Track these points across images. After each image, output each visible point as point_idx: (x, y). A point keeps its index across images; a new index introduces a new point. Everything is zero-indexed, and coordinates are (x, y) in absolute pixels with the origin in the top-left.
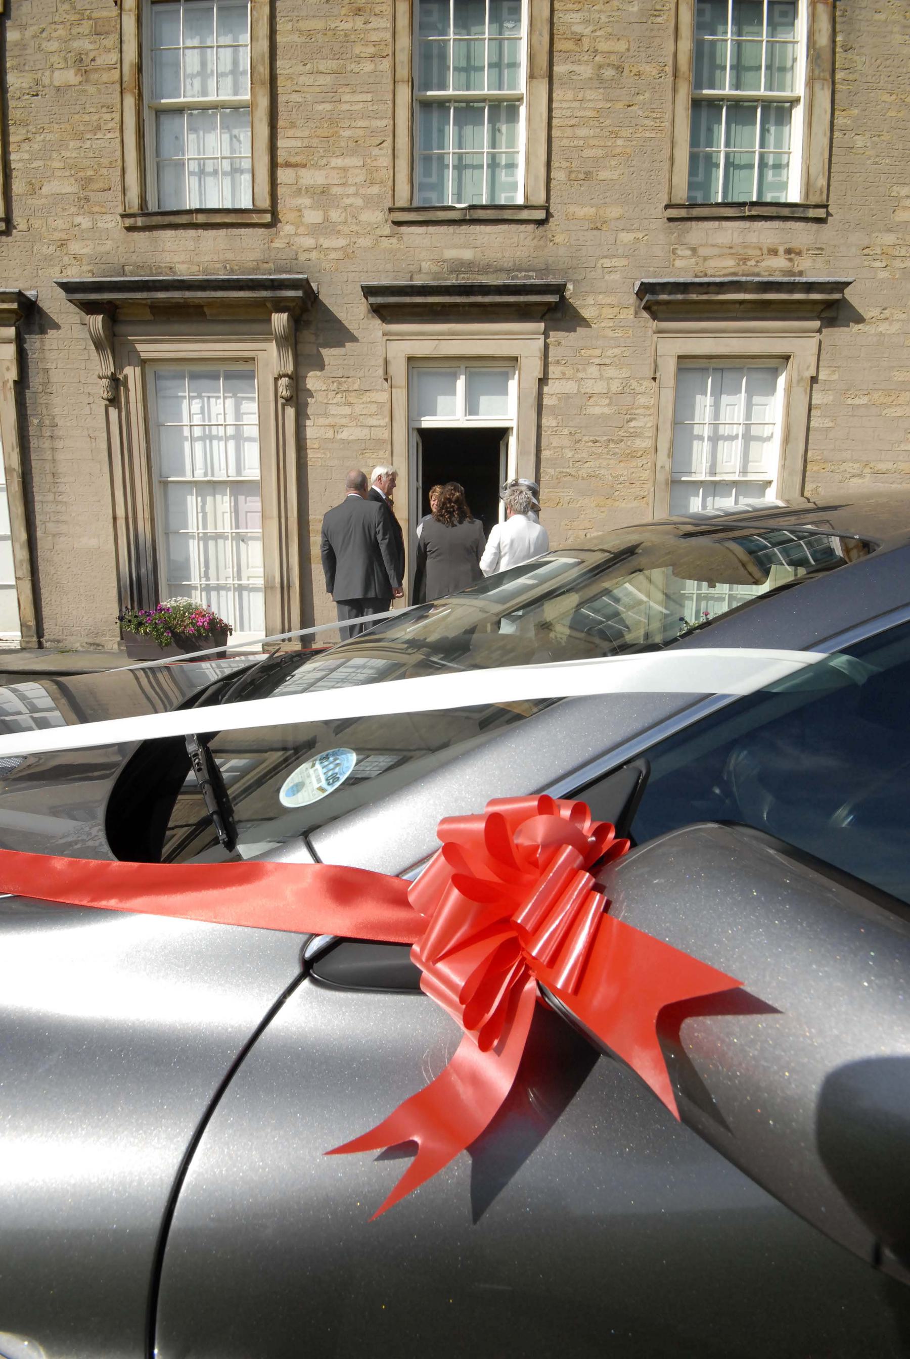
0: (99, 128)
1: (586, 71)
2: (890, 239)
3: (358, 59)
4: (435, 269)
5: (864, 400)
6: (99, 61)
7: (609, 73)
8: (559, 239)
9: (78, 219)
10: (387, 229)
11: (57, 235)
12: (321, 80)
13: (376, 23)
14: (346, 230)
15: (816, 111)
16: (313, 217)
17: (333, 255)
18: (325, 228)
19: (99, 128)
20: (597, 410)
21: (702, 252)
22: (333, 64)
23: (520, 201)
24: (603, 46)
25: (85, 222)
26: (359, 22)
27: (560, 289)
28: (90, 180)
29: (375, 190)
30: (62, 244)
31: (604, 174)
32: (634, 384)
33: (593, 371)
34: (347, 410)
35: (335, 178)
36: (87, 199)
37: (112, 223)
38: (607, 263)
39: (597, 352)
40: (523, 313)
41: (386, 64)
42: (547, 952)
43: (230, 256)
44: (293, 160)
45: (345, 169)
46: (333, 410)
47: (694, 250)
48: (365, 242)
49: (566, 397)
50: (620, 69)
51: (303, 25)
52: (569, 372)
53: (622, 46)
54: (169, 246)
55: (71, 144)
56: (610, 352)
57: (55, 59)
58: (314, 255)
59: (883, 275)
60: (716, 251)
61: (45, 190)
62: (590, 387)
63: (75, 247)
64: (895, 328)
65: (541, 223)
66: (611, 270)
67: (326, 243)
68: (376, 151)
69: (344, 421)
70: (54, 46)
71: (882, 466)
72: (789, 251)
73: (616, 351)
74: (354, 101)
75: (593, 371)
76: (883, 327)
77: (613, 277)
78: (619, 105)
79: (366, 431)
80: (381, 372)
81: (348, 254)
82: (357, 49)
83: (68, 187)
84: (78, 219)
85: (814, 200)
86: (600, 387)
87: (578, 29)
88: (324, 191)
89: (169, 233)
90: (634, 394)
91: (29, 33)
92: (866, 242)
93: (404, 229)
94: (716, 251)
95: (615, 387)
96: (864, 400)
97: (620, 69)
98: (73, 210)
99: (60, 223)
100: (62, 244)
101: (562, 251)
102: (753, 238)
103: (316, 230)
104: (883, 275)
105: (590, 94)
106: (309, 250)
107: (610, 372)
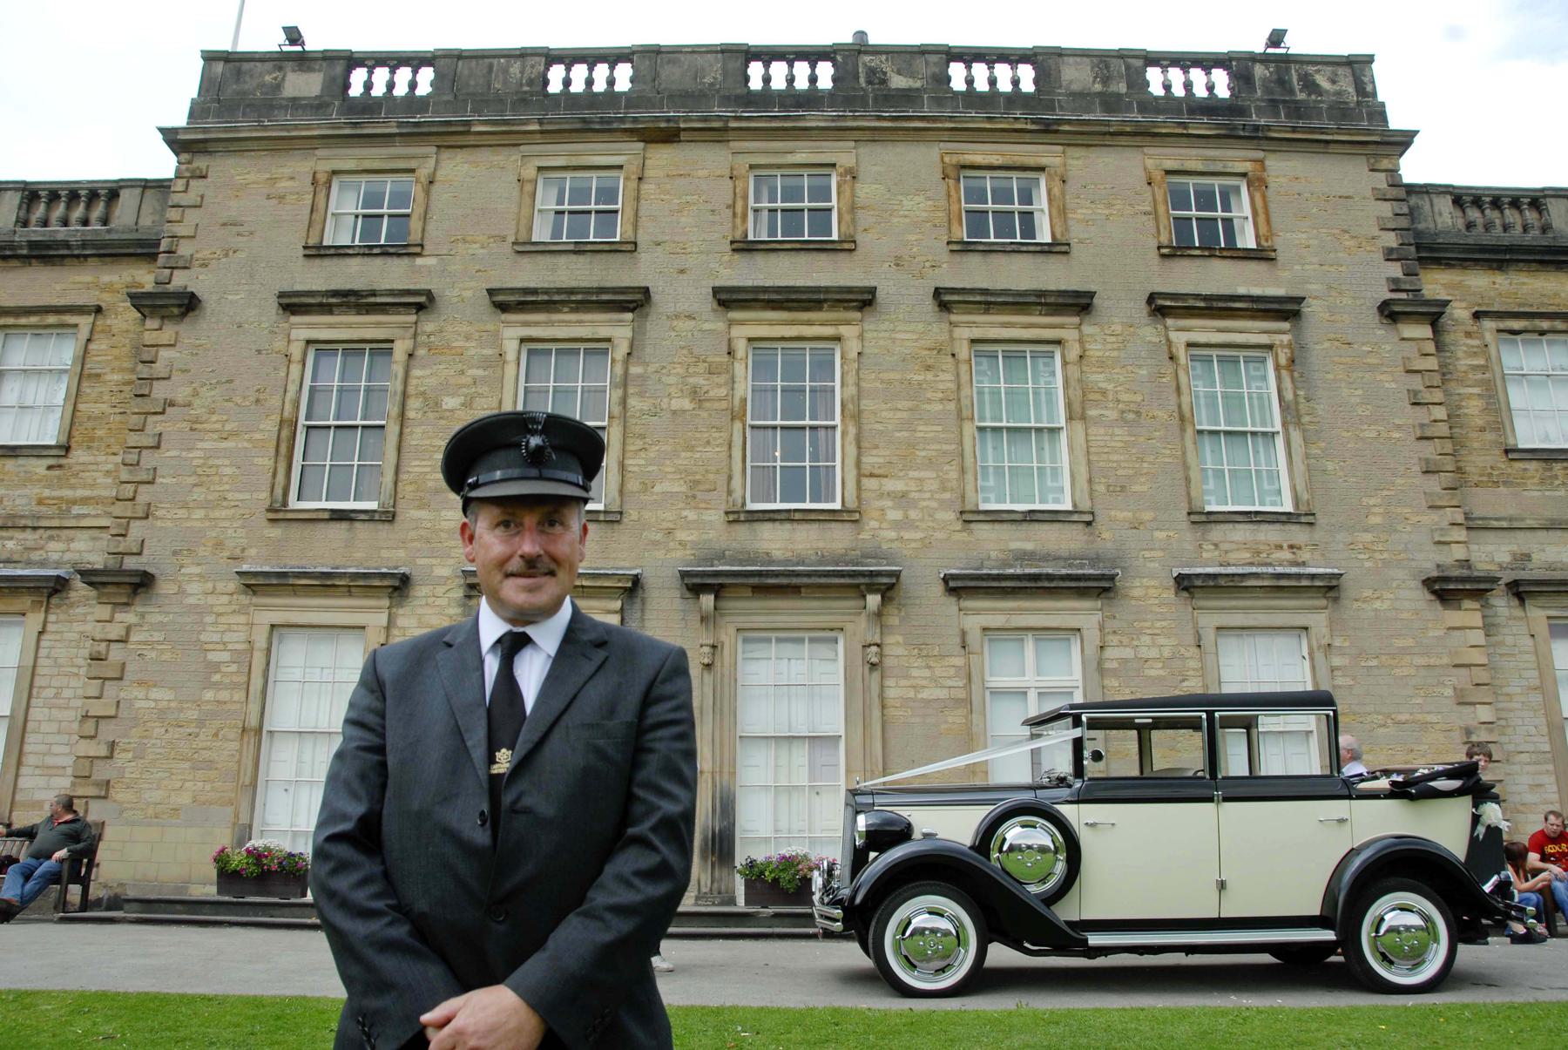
0: (708, 443)
1: (1112, 415)
2: (1368, 537)
3: (929, 401)
4: (1001, 556)
5: (1374, 663)
6: (711, 394)
7: (1131, 416)
8: (1106, 535)
9: (685, 513)
10: (959, 526)
11: (665, 525)
12: (899, 415)
13: (943, 376)
14: (924, 525)
15: (1293, 445)
16: (895, 515)
17: (913, 545)
18: (906, 524)
19: (708, 443)
20: (1153, 673)
21: (1224, 546)
22: (910, 404)
23: (1069, 507)
24: (1124, 397)
25: (691, 515)
26: (929, 376)
27: (1112, 578)
28: (697, 482)
29: (947, 496)
30: (669, 532)
31: (1136, 488)
32: (1183, 650)
33: (1146, 639)
34: (927, 673)
35: (913, 486)
36: (694, 497)
37: (716, 516)
38: (1147, 554)
39: (1148, 624)
40: (1082, 593)
41: (952, 406)
42: (795, 618)
43: (821, 545)
44: (876, 472)
45: (920, 480)
46: (915, 673)
47: (1216, 545)
48: (940, 535)
49: (1124, 661)
50: (1138, 413)
51: (884, 376)
52: (1125, 640)
53: (1139, 398)
54: (766, 535)
55: (683, 454)
56: (1158, 624)
57: (673, 390)
58: (895, 545)
59: (1367, 564)
60: (1234, 546)
61: (658, 488)
62: (1145, 653)
63: (681, 535)
64: (1386, 605)
65: (1089, 523)
66: (1152, 559)
67: (907, 535)
68: (947, 467)
69: (924, 683)
70: (672, 380)
71: (1403, 718)
72: (1291, 547)
73: (1164, 624)
74: (923, 431)
75: (1146, 639)
76: (1377, 604)
77: (1152, 565)
78: (1142, 439)
79: (945, 691)
80: (958, 640)
81: (926, 544)
82: (929, 395)
83: (679, 487)
84: (685, 513)
85: (1303, 509)
86: (1153, 653)
87: (1103, 385)
88: (904, 495)
89: (769, 525)
90: (1183, 658)
91: (651, 369)
92: (1350, 540)
93: (973, 526)
94: (1234, 546)
95: (1166, 653)
96: (1374, 663)
97: (1138, 413)
98: (681, 505)
99: (668, 515)
100: (669, 532)
101: (1109, 545)
102: (1261, 537)
103: (897, 525)
104: (1367, 564)
105: (1117, 431)
106: (892, 541)
107: (1161, 640)
